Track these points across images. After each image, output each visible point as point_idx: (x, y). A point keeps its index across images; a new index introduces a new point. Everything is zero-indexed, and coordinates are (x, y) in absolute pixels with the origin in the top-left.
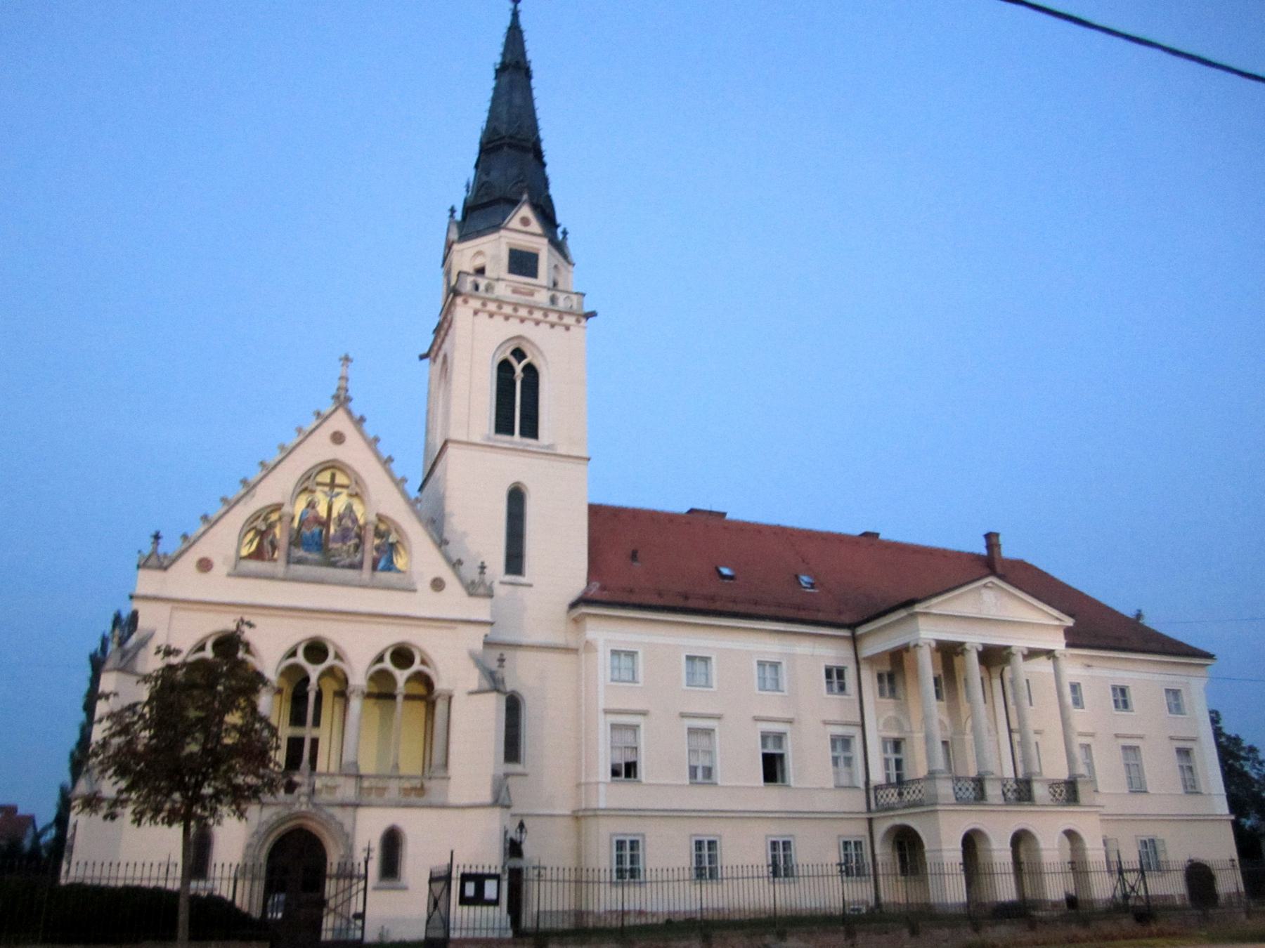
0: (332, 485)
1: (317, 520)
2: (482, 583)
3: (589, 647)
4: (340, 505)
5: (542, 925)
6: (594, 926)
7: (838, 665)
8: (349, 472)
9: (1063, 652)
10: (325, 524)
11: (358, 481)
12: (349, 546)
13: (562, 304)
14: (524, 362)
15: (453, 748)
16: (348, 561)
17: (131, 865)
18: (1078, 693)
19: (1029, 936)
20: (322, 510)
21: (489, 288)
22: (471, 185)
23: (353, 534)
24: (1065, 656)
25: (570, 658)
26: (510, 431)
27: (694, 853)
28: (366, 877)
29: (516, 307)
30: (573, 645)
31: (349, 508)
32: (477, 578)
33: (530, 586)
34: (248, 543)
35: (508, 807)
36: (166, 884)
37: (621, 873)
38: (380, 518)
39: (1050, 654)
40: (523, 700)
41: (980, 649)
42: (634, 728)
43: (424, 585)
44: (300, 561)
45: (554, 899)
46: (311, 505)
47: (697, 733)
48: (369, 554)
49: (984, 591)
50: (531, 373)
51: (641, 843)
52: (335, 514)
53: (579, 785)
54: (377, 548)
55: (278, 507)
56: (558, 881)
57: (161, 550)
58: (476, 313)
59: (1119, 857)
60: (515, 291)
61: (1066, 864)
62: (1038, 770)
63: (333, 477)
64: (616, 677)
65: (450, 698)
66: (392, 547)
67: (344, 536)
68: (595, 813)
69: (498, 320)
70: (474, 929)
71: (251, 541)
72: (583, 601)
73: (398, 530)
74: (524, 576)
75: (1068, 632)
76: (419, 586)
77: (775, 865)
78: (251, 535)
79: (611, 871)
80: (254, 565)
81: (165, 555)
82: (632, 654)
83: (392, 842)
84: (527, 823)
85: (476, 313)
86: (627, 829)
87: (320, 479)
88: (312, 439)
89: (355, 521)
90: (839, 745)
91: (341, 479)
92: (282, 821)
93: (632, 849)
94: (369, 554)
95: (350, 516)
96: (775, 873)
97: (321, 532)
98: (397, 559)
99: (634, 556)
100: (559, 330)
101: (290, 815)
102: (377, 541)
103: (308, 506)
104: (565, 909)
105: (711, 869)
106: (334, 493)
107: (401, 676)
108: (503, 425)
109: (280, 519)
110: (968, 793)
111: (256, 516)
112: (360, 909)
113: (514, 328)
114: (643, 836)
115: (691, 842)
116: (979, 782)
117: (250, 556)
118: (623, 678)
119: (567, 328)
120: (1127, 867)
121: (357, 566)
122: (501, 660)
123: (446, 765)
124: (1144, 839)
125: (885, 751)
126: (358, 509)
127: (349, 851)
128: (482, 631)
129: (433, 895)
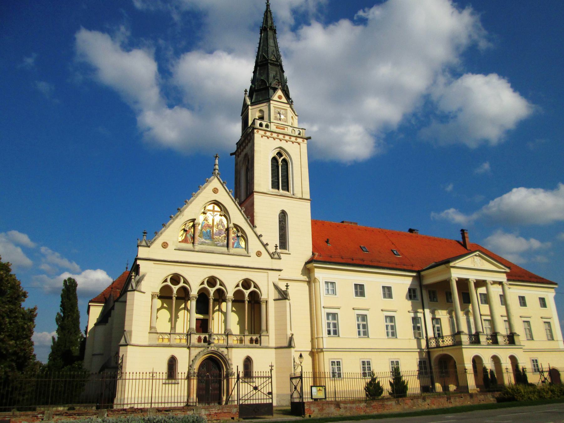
1: (209, 226)
7: (413, 288)
9: (506, 282)
12: (222, 237)
14: (282, 158)
17: (135, 373)
19: (74, 421)
21: (267, 126)
24: (507, 285)
27: (362, 366)
28: (271, 377)
34: (181, 236)
36: (546, 371)
39: (500, 283)
41: (475, 281)
45: (176, 391)
46: (206, 219)
49: (475, 257)
52: (215, 224)
56: (410, 376)
59: (549, 366)
60: (277, 128)
61: (416, 372)
62: (211, 328)
65: (267, 302)
70: (331, 398)
71: (182, 235)
75: (508, 274)
77: (334, 373)
79: (330, 373)
80: (184, 245)
83: (248, 362)
86: (335, 356)
90: (330, 317)
95: (222, 224)
96: (334, 376)
99: (327, 242)
103: (204, 220)
104: (269, 391)
105: (338, 373)
106: (214, 214)
107: (175, 288)
108: (275, 185)
110: (447, 339)
112: (270, 391)
113: (278, 143)
115: (360, 361)
116: (477, 335)
117: (182, 241)
119: (299, 144)
120: (545, 370)
122: (287, 286)
124: (533, 359)
125: (358, 320)
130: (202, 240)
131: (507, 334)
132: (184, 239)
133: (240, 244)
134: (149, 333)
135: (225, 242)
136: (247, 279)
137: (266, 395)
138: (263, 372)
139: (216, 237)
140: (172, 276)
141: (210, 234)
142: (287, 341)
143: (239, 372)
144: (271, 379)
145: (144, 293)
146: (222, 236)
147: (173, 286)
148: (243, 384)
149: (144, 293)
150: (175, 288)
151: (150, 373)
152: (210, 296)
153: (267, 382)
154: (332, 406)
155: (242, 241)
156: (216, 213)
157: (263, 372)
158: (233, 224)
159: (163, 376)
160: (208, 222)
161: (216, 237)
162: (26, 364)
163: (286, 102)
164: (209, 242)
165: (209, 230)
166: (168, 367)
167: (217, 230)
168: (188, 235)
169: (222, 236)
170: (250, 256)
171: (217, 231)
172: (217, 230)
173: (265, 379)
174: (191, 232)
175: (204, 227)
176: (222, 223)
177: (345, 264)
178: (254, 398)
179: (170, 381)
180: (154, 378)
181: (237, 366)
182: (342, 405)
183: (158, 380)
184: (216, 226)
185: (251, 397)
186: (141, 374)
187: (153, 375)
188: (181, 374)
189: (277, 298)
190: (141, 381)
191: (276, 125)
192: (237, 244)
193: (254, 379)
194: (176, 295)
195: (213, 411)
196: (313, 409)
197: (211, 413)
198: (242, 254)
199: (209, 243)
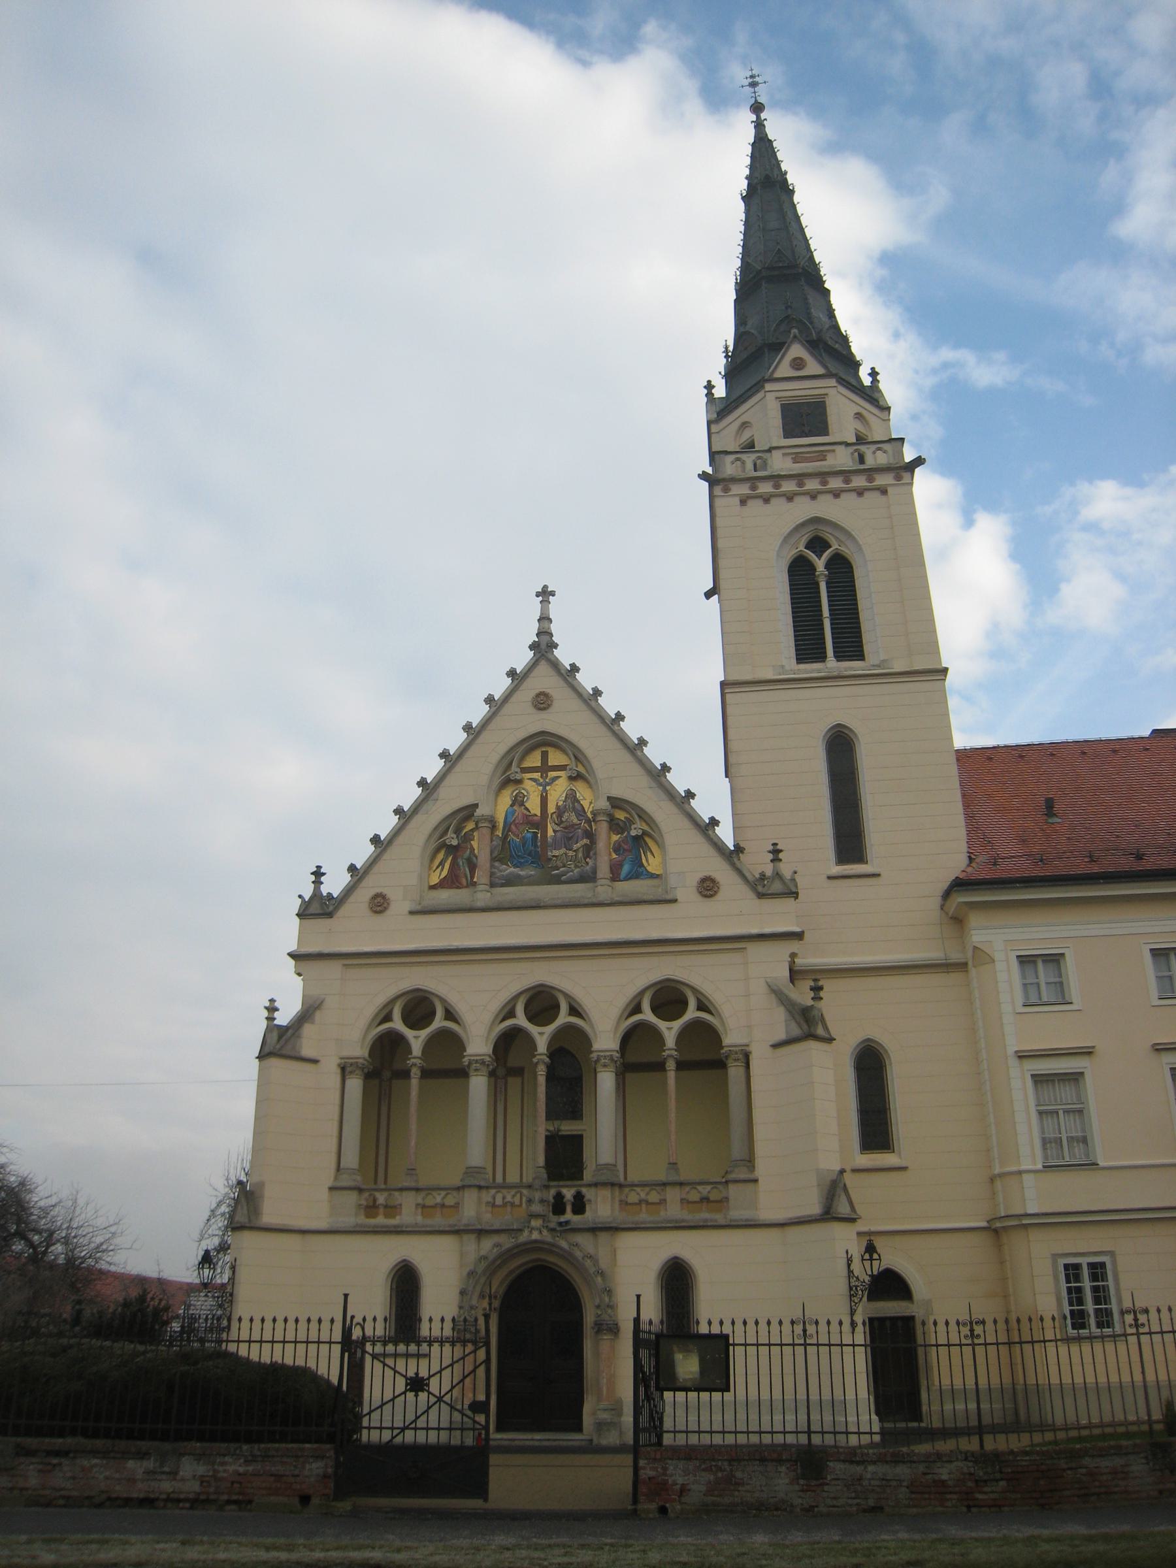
0: (545, 768)
1: (529, 820)
3: (981, 956)
4: (558, 793)
8: (564, 745)
10: (539, 824)
11: (578, 756)
13: (870, 461)
14: (826, 555)
15: (760, 1132)
18: (1086, 1319)
20: (533, 805)
22: (731, 348)
25: (955, 977)
29: (800, 478)
30: (955, 957)
31: (572, 796)
32: (769, 870)
33: (877, 875)
34: (437, 867)
35: (852, 1220)
37: (1079, 1319)
38: (616, 803)
40: (886, 1051)
42: (1076, 1078)
43: (686, 892)
44: (509, 882)
46: (519, 801)
47: (1053, 1081)
48: (603, 860)
50: (841, 568)
51: (1109, 1266)
52: (551, 809)
53: (992, 1180)
54: (617, 849)
55: (468, 812)
57: (325, 890)
58: (743, 502)
60: (795, 461)
63: (545, 756)
64: (1034, 999)
65: (747, 1056)
66: (639, 842)
67: (567, 838)
68: (1026, 1223)
69: (778, 504)
71: (442, 864)
72: (960, 884)
73: (643, 815)
74: (867, 863)
76: (680, 894)
78: (441, 856)
80: (445, 896)
82: (1055, 960)
84: (879, 1243)
85: (743, 502)
87: (528, 763)
88: (508, 709)
89: (581, 813)
91: (555, 758)
92: (506, 1256)
93: (1094, 1277)
94: (603, 860)
97: (535, 834)
100: (872, 498)
101: (517, 1246)
102: (615, 838)
109: (477, 828)
111: (442, 828)
113: (803, 509)
114: (1112, 1254)
118: (1045, 999)
121: (588, 878)
123: (749, 1161)
126: (585, 796)
128: (782, 950)
133: (642, 865)
134: (331, 1189)
135: (587, 863)
136: (668, 980)
137: (463, 1414)
138: (757, 1323)
139: (556, 853)
140: (653, 995)
141: (536, 846)
143: (353, 1317)
144: (483, 1349)
145: (315, 1061)
146: (575, 847)
147: (662, 1025)
148: (409, 1361)
149: (315, 1061)
150: (668, 1028)
151: (793, 1323)
153: (469, 1361)
154: (783, 1469)
156: (552, 774)
157: (757, 1323)
158: (609, 798)
159: (296, 1330)
160: (527, 809)
161: (556, 853)
163: (820, 370)
164: (532, 873)
165: (529, 835)
166: (667, 1299)
167: (558, 828)
169: (575, 847)
170: (675, 901)
171: (559, 834)
172: (558, 828)
173: (447, 1348)
175: (513, 827)
177: (1099, 878)
178: (433, 1423)
179: (402, 1348)
180: (808, 1341)
181: (638, 1297)
182: (837, 1468)
183: (824, 1350)
184: (554, 816)
185: (417, 1418)
186: (314, 1325)
187: (805, 1331)
188: (428, 1323)
189: (781, 1035)
190: (764, 1350)
191: (795, 453)
193: (424, 1347)
194: (676, 1050)
195: (228, 1468)
196: (680, 1481)
197: (218, 1472)
198: (645, 898)
199: (531, 875)
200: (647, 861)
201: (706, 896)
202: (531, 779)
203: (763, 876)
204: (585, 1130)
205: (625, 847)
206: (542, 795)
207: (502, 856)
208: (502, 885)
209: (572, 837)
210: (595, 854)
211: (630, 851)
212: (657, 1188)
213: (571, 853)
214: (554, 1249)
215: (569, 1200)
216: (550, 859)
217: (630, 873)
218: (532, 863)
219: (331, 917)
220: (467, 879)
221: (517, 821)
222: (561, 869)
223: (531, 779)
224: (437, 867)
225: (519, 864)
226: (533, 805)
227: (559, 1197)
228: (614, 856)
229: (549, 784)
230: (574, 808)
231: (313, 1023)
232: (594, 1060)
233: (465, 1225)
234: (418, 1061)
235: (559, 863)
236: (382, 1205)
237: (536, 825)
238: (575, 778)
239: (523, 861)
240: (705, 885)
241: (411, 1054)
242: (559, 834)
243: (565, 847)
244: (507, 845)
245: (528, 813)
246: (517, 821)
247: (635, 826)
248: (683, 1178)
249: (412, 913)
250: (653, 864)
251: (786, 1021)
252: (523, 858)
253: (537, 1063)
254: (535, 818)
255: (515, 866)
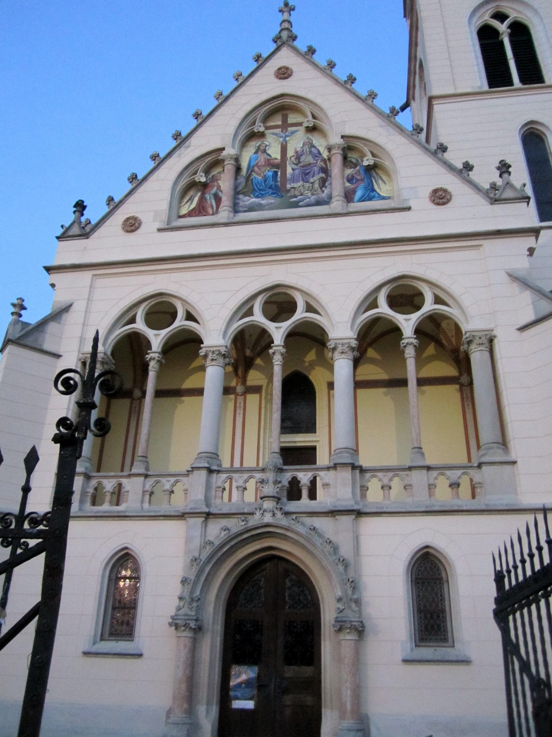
1: (270, 163)
2: (508, 183)
5: (351, 358)
6: (315, 369)
10: (281, 165)
14: (507, 22)
15: (510, 414)
16: (313, 198)
23: (316, 169)
26: (507, 81)
34: (187, 202)
52: (290, 153)
65: (491, 341)
67: (305, 174)
81: (88, 222)
97: (276, 173)
98: (379, 187)
123: (504, 443)
126: (320, 143)
127: (350, 592)
129: (525, 667)
130: (249, 202)
131: (247, 669)
132: (194, 208)
133: (373, 190)
139: (293, 185)
142: (28, 663)
146: (312, 180)
152: (402, 339)
155: (380, 182)
156: (290, 129)
160: (269, 155)
161: (293, 185)
162: (251, 661)
164: (272, 201)
165: (270, 174)
168: (207, 196)
170: (409, 209)
171: (297, 172)
174: (215, 189)
176: (310, 148)
184: (293, 158)
192: (366, 189)
199: (271, 203)
200: (379, 187)
201: (438, 204)
202: (273, 134)
203: (494, 187)
204: (318, 441)
205: (358, 178)
206: (282, 144)
207: (245, 190)
208: (245, 211)
209: (309, 172)
210: (331, 184)
211: (363, 180)
212: (401, 473)
213: (307, 185)
214: (289, 534)
215: (305, 485)
216: (289, 190)
217: (362, 197)
218: (272, 193)
219: (87, 238)
220: (213, 209)
221: (259, 164)
222: (299, 197)
223: (273, 134)
224: (187, 202)
225: (260, 195)
226: (275, 153)
227: (295, 483)
228: (348, 184)
229: (288, 136)
230: (311, 152)
231: (59, 323)
232: (331, 347)
233: (191, 509)
234: (156, 355)
235: (297, 193)
236: (109, 492)
237: (277, 166)
238: (312, 129)
239: (263, 193)
240: (437, 194)
241: (151, 349)
242: (297, 172)
243: (303, 180)
244: (250, 182)
245: (269, 158)
246: (259, 164)
247: (367, 158)
248: (429, 462)
249: (159, 230)
250: (382, 189)
251: (533, 303)
252: (264, 190)
253: (274, 353)
254: (276, 161)
255: (257, 197)
